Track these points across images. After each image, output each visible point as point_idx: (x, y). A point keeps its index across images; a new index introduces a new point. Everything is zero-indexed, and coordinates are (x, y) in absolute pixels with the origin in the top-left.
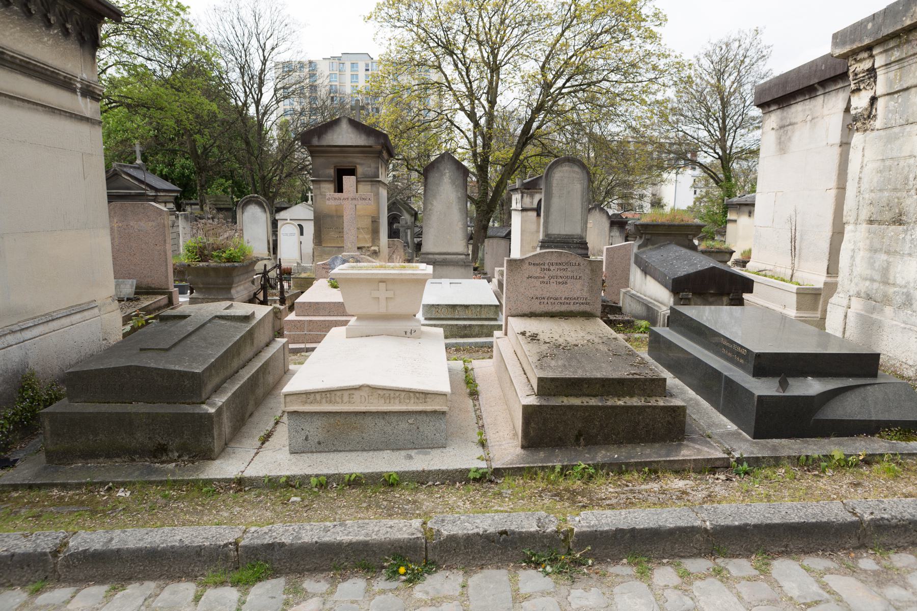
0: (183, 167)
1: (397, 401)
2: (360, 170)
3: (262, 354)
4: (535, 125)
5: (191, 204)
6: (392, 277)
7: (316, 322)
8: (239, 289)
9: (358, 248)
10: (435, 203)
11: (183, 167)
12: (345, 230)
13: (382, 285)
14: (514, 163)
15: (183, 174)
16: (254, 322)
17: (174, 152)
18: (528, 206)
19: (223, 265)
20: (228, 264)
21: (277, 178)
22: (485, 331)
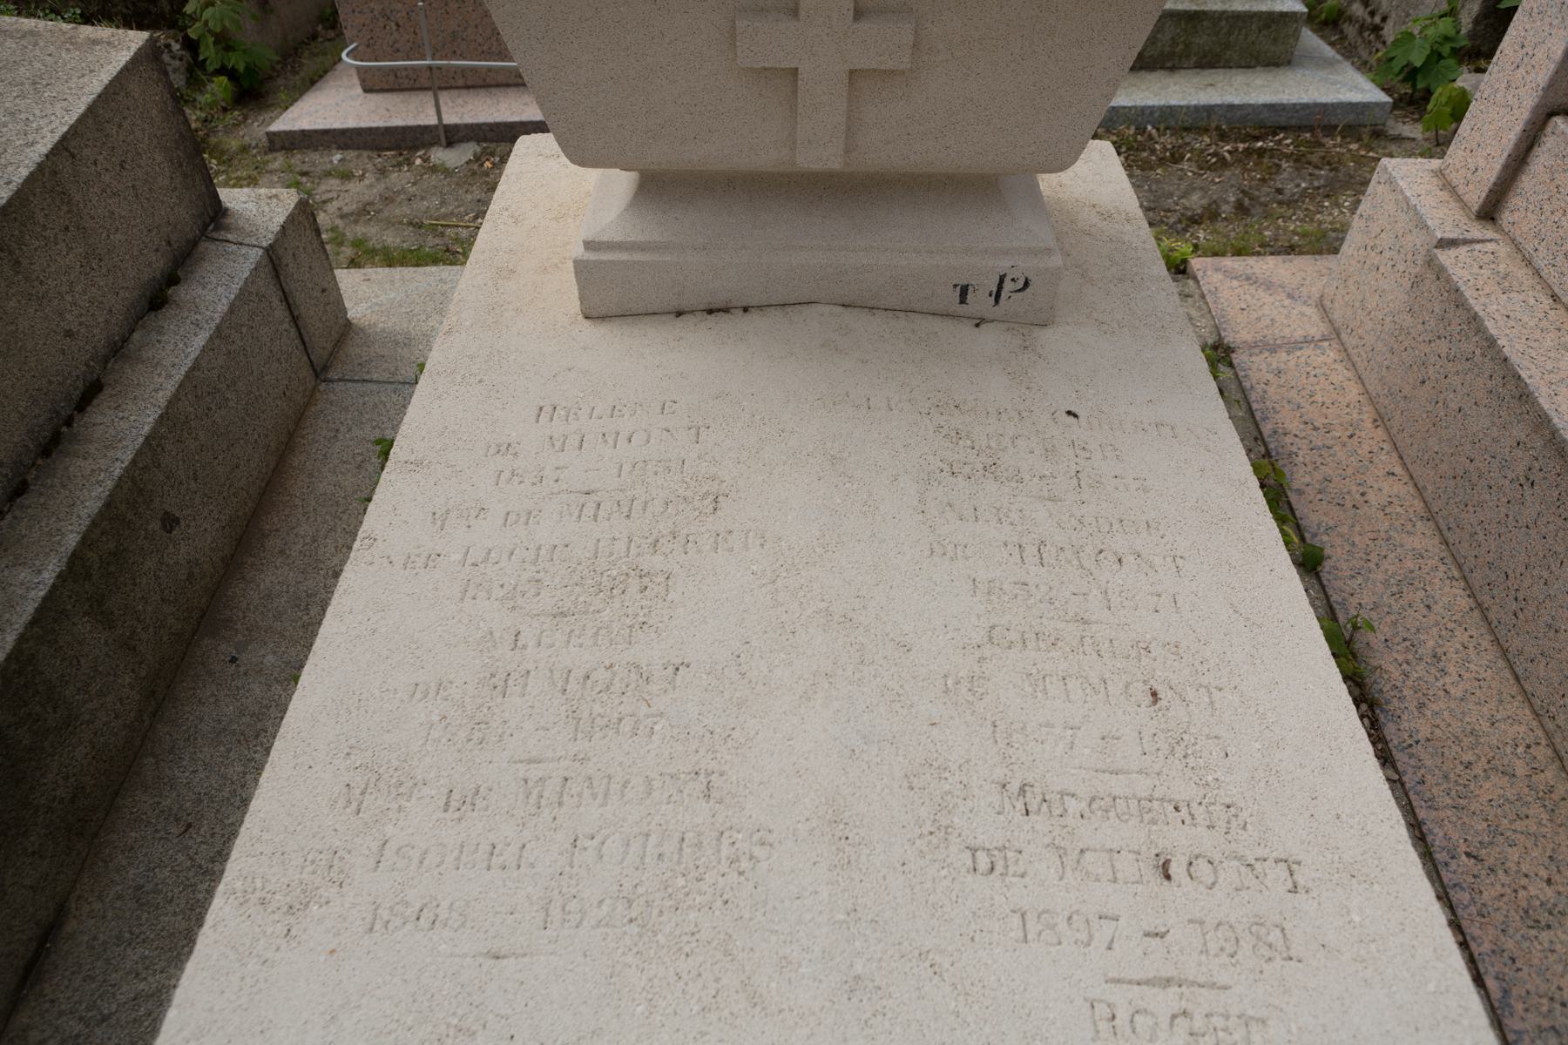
22: (1202, 40)
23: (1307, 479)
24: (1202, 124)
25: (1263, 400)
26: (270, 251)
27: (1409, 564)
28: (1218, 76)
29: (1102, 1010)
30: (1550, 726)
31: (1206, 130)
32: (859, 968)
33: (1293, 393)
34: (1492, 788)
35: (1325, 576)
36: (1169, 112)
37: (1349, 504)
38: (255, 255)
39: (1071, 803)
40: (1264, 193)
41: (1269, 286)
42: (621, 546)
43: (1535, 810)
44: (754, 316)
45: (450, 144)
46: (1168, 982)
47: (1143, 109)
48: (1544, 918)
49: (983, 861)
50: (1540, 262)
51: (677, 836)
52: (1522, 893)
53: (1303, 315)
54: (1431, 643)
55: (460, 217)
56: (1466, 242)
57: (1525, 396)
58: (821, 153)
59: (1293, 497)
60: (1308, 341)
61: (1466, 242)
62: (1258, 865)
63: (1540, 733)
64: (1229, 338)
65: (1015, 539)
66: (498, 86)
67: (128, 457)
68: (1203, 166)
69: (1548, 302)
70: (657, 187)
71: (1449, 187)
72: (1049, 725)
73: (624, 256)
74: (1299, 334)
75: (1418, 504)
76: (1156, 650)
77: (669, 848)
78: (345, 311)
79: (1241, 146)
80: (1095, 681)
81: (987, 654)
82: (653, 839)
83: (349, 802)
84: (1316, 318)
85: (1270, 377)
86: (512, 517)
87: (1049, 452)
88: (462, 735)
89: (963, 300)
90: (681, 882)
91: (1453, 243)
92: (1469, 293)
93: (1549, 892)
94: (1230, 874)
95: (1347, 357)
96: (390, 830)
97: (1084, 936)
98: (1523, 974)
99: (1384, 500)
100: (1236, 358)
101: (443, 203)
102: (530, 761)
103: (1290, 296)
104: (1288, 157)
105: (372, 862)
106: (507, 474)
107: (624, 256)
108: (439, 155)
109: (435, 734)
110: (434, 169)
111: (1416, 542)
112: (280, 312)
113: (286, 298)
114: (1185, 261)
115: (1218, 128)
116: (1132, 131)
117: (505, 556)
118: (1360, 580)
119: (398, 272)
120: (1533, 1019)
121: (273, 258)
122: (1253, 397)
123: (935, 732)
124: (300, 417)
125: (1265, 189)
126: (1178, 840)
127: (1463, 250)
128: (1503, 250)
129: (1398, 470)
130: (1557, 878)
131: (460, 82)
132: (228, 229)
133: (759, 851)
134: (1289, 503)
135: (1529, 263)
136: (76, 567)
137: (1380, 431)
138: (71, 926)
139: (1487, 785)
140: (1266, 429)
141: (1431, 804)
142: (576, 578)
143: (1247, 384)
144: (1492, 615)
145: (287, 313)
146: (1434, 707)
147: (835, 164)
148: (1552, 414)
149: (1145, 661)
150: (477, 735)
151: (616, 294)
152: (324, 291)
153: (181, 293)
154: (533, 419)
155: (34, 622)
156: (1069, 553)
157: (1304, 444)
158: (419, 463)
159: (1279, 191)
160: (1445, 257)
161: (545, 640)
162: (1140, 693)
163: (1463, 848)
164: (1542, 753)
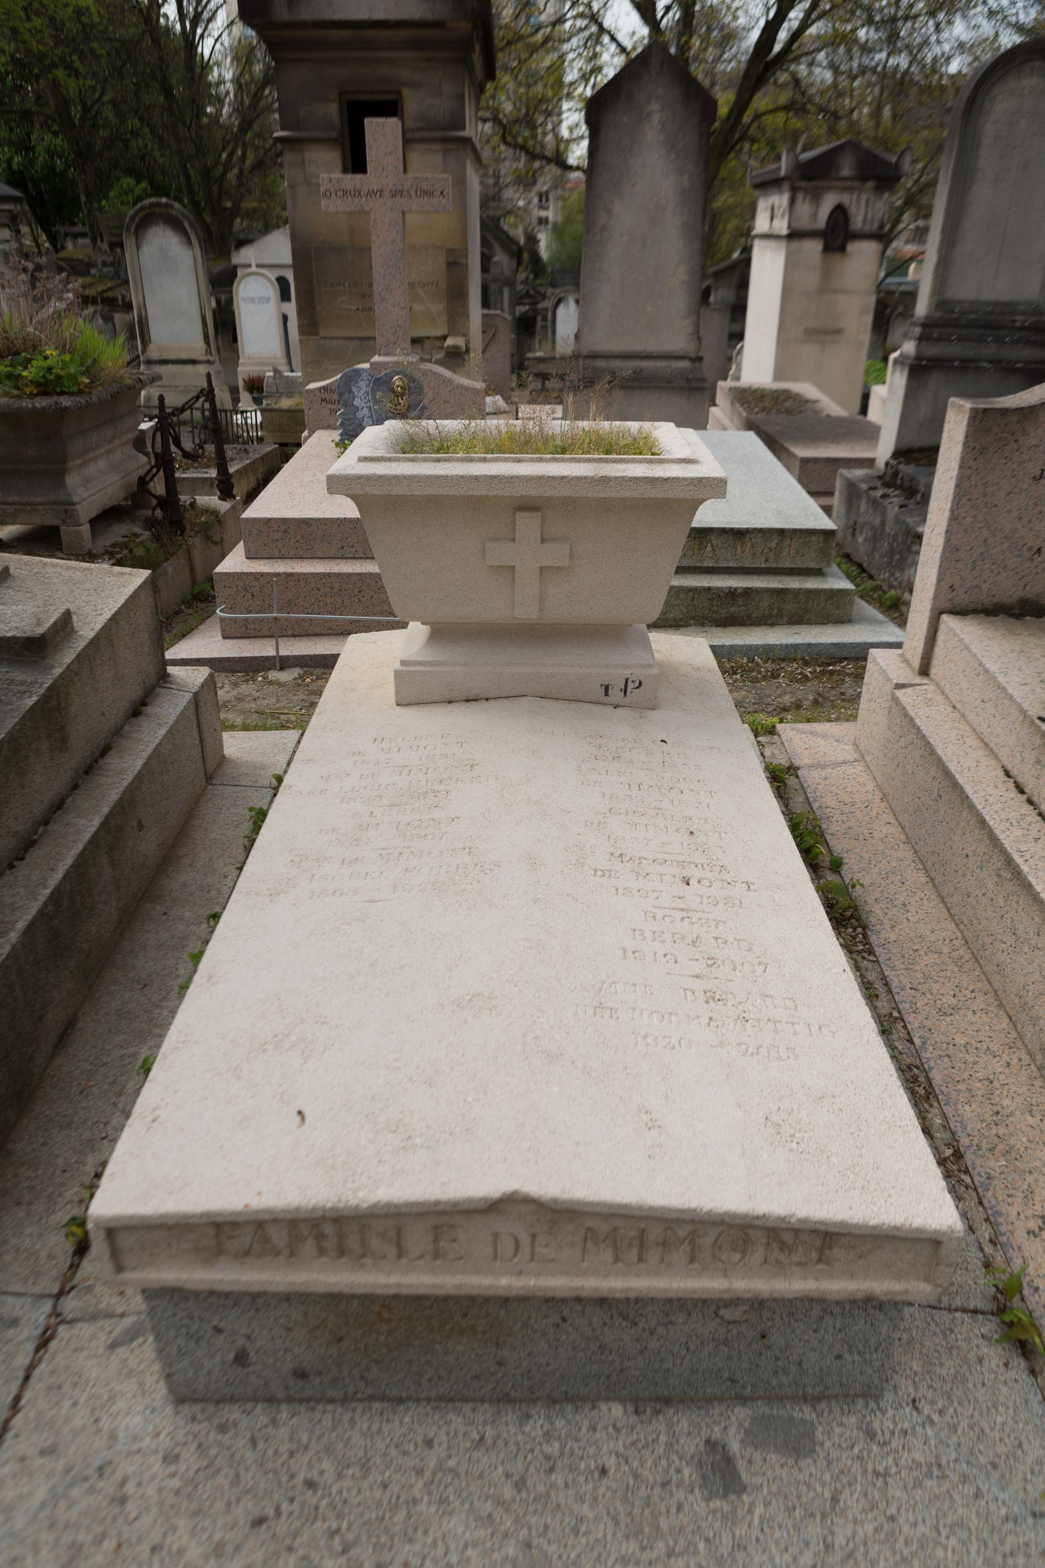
0: (50, 153)
1: (679, 1256)
2: (412, 103)
3: (113, 761)
4: (783, 35)
5: (75, 236)
6: (566, 492)
7: (303, 612)
8: (92, 470)
9: (415, 341)
10: (617, 207)
11: (50, 153)
12: (378, 288)
13: (528, 525)
14: (732, 130)
15: (53, 168)
16: (68, 657)
17: (26, 116)
18: (804, 223)
19: (27, 403)
20: (42, 402)
21: (236, 171)
22: (789, 607)
24: (792, 656)
26: (196, 694)
28: (796, 628)
31: (795, 660)
35: (843, 873)
36: (768, 649)
38: (188, 696)
40: (832, 695)
41: (824, 736)
44: (492, 703)
45: (282, 669)
47: (750, 646)
50: (947, 691)
55: (290, 709)
56: (911, 685)
57: (933, 752)
58: (526, 611)
59: (828, 837)
61: (911, 685)
64: (797, 763)
66: (315, 635)
67: (130, 778)
68: (793, 679)
69: (950, 709)
70: (442, 633)
71: (906, 661)
73: (422, 668)
74: (840, 759)
75: (903, 837)
79: (818, 669)
89: (607, 694)
91: (903, 686)
92: (909, 708)
93: (954, 1001)
99: (883, 835)
101: (278, 701)
104: (850, 675)
107: (422, 668)
108: (273, 675)
110: (271, 683)
111: (900, 854)
112: (195, 733)
113: (199, 726)
114: (774, 727)
115: (803, 659)
116: (745, 660)
119: (252, 734)
120: (937, 1052)
121: (196, 700)
122: (808, 791)
125: (833, 693)
126: (694, 873)
127: (909, 690)
128: (931, 688)
129: (893, 821)
130: (958, 994)
131: (290, 633)
132: (171, 683)
135: (943, 693)
136: (105, 825)
137: (884, 804)
138: (80, 1025)
140: (815, 806)
147: (535, 616)
151: (414, 691)
153: (148, 710)
155: (90, 842)
157: (838, 812)
158: (310, 760)
159: (843, 694)
160: (899, 693)
164: (959, 943)
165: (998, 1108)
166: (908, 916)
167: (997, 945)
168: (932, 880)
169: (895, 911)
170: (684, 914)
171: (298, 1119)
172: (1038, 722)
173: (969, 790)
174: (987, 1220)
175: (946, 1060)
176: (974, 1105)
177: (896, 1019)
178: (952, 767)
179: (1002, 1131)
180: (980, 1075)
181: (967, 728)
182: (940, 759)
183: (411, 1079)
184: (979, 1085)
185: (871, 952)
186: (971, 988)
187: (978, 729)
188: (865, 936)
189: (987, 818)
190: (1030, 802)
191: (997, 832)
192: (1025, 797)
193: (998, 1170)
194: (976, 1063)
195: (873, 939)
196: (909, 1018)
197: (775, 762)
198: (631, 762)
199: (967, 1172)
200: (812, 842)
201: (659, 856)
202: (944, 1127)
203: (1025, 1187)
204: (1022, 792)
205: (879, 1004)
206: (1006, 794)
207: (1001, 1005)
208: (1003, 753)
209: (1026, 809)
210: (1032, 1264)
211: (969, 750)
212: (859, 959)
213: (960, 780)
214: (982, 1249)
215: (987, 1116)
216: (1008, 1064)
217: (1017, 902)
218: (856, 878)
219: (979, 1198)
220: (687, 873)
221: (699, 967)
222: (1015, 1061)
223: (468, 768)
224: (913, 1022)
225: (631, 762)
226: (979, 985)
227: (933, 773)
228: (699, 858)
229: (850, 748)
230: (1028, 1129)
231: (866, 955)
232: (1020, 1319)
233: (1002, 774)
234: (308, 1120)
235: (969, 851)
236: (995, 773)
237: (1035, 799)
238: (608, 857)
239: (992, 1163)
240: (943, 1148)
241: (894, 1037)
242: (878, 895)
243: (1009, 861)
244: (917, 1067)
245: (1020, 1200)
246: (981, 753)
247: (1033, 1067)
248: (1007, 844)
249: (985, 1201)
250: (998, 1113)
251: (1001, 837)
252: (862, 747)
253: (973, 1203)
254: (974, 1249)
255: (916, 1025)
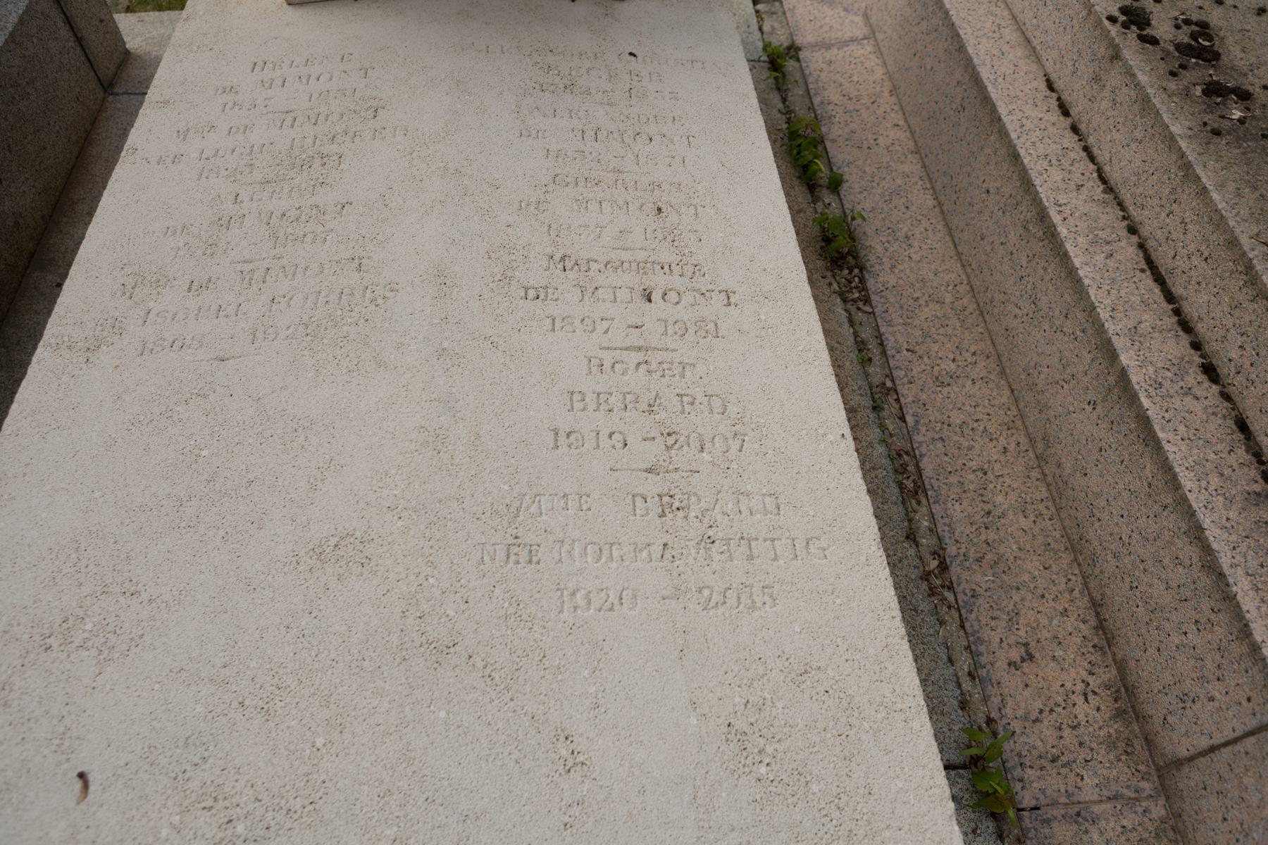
23: (840, 132)
25: (817, 81)
27: (899, 182)
29: (595, 362)
30: (969, 271)
32: (445, 345)
33: (838, 76)
34: (929, 311)
35: (842, 193)
37: (865, 146)
39: (594, 266)
42: (309, 141)
43: (954, 322)
46: (640, 348)
48: (947, 380)
49: (532, 293)
51: (339, 291)
52: (937, 368)
53: (852, 22)
54: (905, 229)
57: (961, 48)
59: (828, 144)
60: (853, 40)
62: (707, 294)
63: (964, 277)
64: (799, 41)
65: (580, 127)
72: (586, 226)
74: (848, 36)
75: (911, 144)
76: (665, 187)
77: (333, 297)
78: (124, 43)
80: (620, 202)
81: (550, 189)
82: (323, 294)
83: (124, 293)
84: (861, 24)
85: (824, 66)
86: (234, 130)
87: (613, 76)
88: (199, 252)
90: (339, 312)
93: (953, 366)
94: (688, 298)
95: (878, 51)
96: (152, 304)
97: (590, 328)
98: (929, 412)
99: (889, 142)
100: (802, 55)
102: (244, 262)
103: (845, 10)
105: (141, 322)
106: (230, 105)
109: (181, 253)
111: (906, 168)
112: (64, 32)
113: (68, 21)
117: (229, 152)
118: (865, 193)
122: (810, 80)
123: (509, 230)
124: (93, 123)
126: (658, 281)
129: (901, 123)
130: (958, 358)
133: (388, 294)
134: (825, 149)
137: (894, 99)
139: (926, 310)
140: (816, 101)
141: (890, 323)
142: (277, 161)
143: (807, 72)
144: (945, 208)
145: (71, 34)
146: (901, 267)
148: (974, 56)
149: (656, 192)
150: (209, 252)
152: (101, 21)
154: (249, 71)
156: (616, 135)
158: (166, 102)
161: (255, 197)
162: (649, 207)
163: (906, 346)
164: (963, 289)
165: (990, 506)
166: (909, 256)
167: (1010, 307)
168: (940, 205)
169: (896, 246)
170: (640, 356)
171: (78, 785)
172: (1106, 22)
173: (1002, 110)
174: (968, 648)
175: (940, 444)
176: (965, 504)
177: (889, 389)
178: (985, 74)
179: (992, 536)
180: (974, 464)
181: (1006, 13)
182: (969, 62)
183: (242, 704)
184: (971, 477)
185: (867, 300)
186: (972, 349)
187: (1020, 17)
188: (862, 280)
189: (1022, 152)
190: (1075, 129)
191: (1033, 174)
192: (1069, 121)
193: (984, 586)
194: (970, 448)
195: (871, 284)
196: (903, 390)
197: (775, 43)
198: (588, 92)
199: (951, 588)
200: (810, 158)
201: (614, 255)
202: (931, 530)
203: (1011, 607)
204: (1066, 113)
205: (871, 370)
206: (1047, 117)
207: (1003, 373)
208: (1049, 57)
209: (1070, 140)
210: (1010, 702)
211: (1006, 48)
212: (853, 309)
213: (994, 94)
214: (959, 685)
215: (977, 518)
216: (1005, 450)
217: (1045, 269)
218: (859, 208)
219: (962, 621)
220: (648, 282)
221: (653, 452)
222: (1012, 447)
223: (370, 113)
224: (908, 394)
225: (588, 92)
226: (982, 346)
227: (958, 75)
228: (666, 256)
229: (858, 19)
230: (1019, 533)
231: (860, 304)
232: (996, 791)
233: (1043, 85)
234: (92, 788)
235: (992, 186)
236: (1035, 84)
237: (1082, 127)
238: (545, 263)
239: (978, 578)
240: (928, 557)
241: (885, 414)
242: (878, 224)
243: (1043, 216)
244: (907, 453)
245: (1003, 624)
246: (1020, 52)
247: (1031, 454)
248: (1043, 192)
249: (967, 625)
250: (989, 513)
251: (1037, 182)
252: (873, 20)
253: (953, 626)
254: (951, 686)
255: (910, 399)
